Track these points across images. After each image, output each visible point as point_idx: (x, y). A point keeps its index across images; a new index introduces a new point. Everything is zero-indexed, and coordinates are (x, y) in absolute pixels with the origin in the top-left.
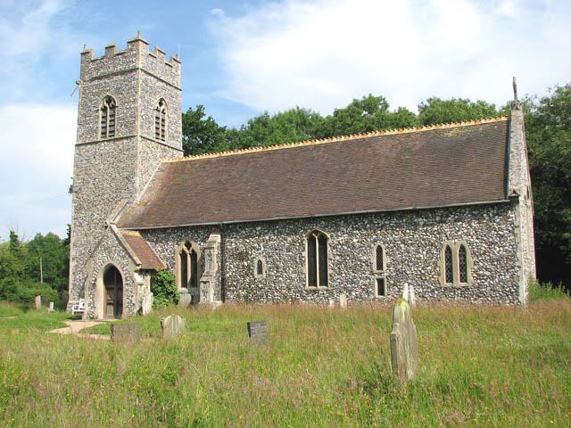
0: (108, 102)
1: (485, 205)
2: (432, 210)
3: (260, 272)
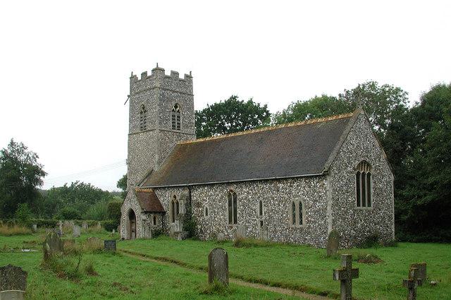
0: (143, 108)
1: (313, 176)
2: (286, 179)
3: (207, 215)
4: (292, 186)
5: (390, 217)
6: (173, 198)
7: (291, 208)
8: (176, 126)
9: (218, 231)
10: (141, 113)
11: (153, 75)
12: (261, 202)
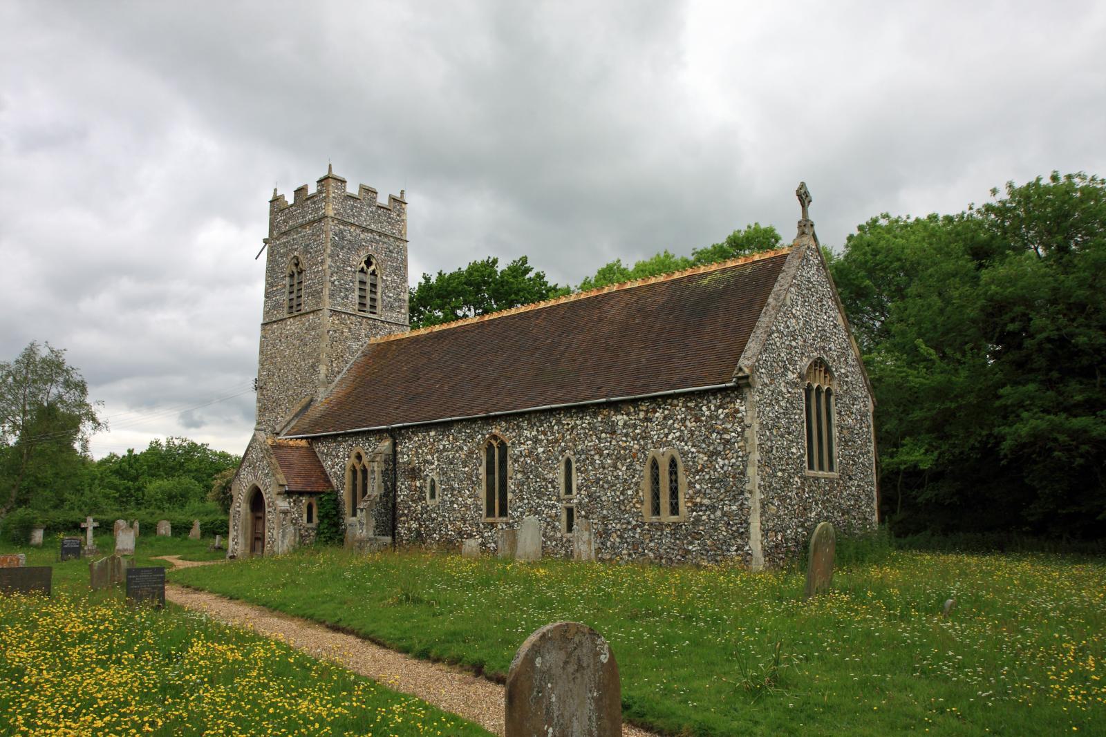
0: (297, 265)
1: (706, 391)
2: (634, 402)
3: (433, 496)
4: (650, 420)
5: (870, 498)
6: (353, 460)
7: (647, 472)
8: (367, 303)
9: (460, 533)
10: (292, 276)
11: (320, 192)
12: (568, 463)
